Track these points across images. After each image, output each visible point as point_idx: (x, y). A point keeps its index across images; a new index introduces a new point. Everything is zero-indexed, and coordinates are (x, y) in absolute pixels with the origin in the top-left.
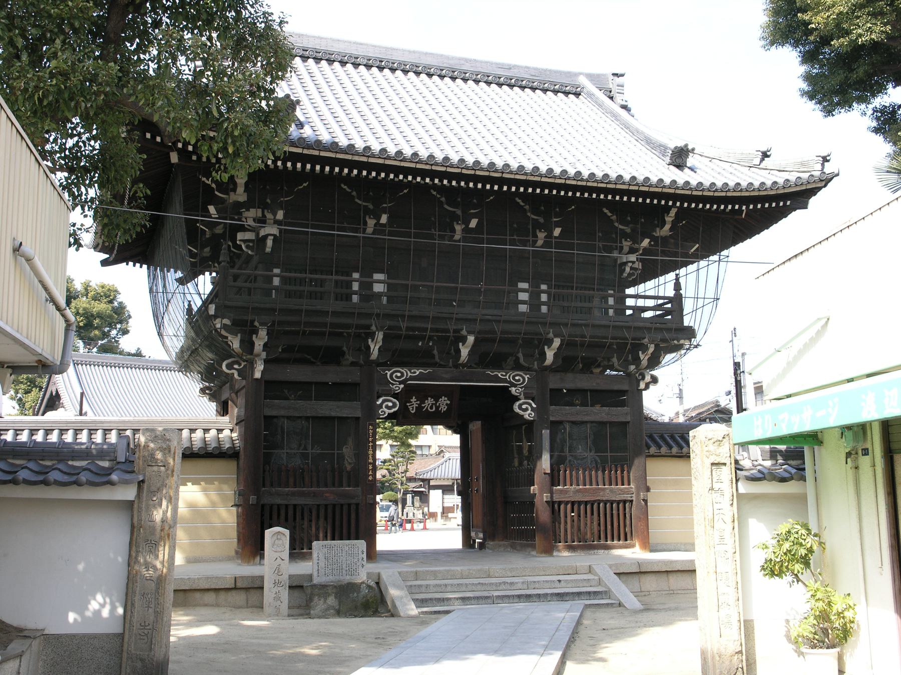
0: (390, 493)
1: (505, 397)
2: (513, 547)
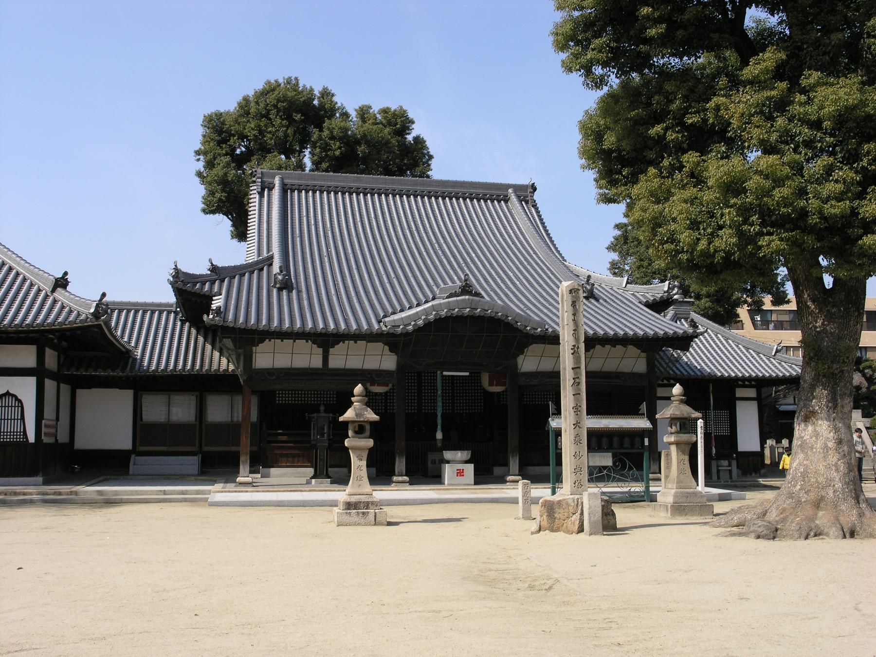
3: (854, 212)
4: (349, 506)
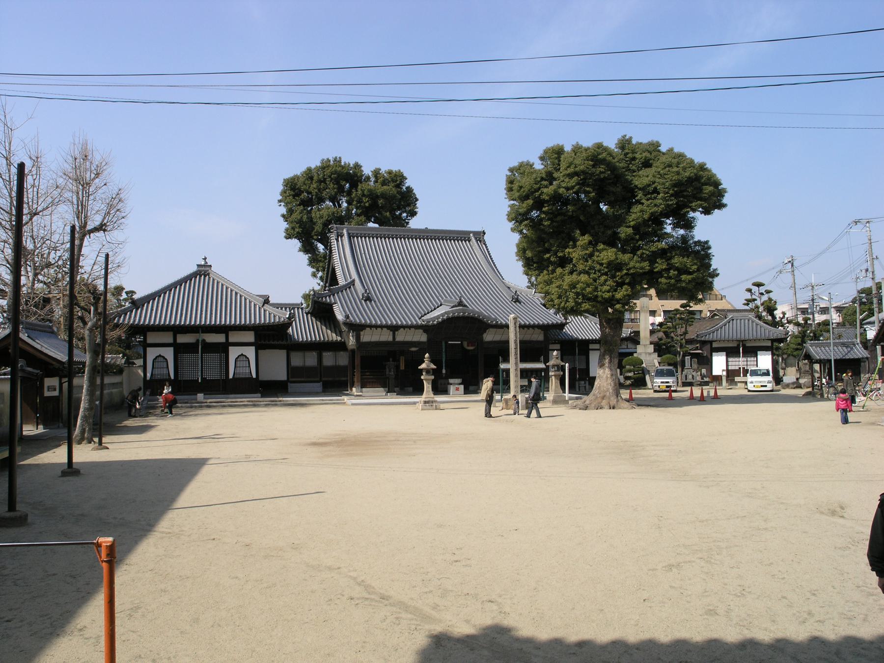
0: (668, 355)
3: (613, 296)
4: (425, 402)
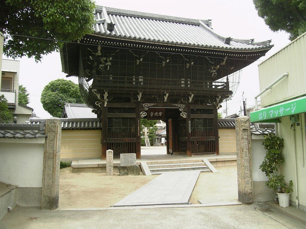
1: (178, 112)
2: (180, 154)
